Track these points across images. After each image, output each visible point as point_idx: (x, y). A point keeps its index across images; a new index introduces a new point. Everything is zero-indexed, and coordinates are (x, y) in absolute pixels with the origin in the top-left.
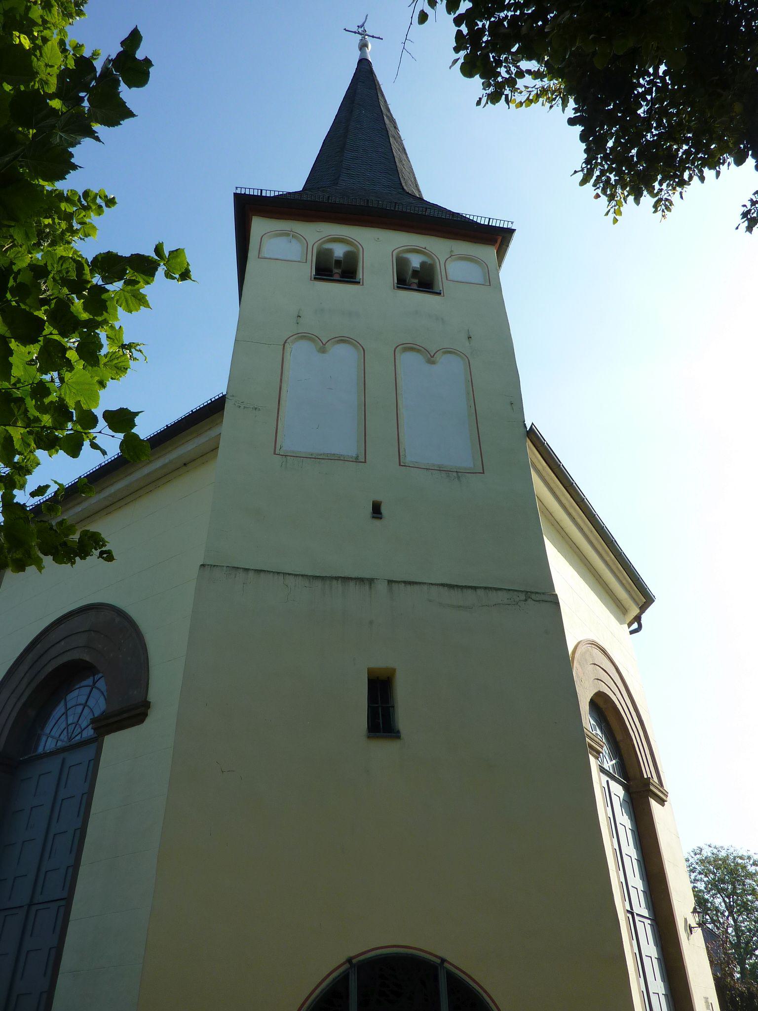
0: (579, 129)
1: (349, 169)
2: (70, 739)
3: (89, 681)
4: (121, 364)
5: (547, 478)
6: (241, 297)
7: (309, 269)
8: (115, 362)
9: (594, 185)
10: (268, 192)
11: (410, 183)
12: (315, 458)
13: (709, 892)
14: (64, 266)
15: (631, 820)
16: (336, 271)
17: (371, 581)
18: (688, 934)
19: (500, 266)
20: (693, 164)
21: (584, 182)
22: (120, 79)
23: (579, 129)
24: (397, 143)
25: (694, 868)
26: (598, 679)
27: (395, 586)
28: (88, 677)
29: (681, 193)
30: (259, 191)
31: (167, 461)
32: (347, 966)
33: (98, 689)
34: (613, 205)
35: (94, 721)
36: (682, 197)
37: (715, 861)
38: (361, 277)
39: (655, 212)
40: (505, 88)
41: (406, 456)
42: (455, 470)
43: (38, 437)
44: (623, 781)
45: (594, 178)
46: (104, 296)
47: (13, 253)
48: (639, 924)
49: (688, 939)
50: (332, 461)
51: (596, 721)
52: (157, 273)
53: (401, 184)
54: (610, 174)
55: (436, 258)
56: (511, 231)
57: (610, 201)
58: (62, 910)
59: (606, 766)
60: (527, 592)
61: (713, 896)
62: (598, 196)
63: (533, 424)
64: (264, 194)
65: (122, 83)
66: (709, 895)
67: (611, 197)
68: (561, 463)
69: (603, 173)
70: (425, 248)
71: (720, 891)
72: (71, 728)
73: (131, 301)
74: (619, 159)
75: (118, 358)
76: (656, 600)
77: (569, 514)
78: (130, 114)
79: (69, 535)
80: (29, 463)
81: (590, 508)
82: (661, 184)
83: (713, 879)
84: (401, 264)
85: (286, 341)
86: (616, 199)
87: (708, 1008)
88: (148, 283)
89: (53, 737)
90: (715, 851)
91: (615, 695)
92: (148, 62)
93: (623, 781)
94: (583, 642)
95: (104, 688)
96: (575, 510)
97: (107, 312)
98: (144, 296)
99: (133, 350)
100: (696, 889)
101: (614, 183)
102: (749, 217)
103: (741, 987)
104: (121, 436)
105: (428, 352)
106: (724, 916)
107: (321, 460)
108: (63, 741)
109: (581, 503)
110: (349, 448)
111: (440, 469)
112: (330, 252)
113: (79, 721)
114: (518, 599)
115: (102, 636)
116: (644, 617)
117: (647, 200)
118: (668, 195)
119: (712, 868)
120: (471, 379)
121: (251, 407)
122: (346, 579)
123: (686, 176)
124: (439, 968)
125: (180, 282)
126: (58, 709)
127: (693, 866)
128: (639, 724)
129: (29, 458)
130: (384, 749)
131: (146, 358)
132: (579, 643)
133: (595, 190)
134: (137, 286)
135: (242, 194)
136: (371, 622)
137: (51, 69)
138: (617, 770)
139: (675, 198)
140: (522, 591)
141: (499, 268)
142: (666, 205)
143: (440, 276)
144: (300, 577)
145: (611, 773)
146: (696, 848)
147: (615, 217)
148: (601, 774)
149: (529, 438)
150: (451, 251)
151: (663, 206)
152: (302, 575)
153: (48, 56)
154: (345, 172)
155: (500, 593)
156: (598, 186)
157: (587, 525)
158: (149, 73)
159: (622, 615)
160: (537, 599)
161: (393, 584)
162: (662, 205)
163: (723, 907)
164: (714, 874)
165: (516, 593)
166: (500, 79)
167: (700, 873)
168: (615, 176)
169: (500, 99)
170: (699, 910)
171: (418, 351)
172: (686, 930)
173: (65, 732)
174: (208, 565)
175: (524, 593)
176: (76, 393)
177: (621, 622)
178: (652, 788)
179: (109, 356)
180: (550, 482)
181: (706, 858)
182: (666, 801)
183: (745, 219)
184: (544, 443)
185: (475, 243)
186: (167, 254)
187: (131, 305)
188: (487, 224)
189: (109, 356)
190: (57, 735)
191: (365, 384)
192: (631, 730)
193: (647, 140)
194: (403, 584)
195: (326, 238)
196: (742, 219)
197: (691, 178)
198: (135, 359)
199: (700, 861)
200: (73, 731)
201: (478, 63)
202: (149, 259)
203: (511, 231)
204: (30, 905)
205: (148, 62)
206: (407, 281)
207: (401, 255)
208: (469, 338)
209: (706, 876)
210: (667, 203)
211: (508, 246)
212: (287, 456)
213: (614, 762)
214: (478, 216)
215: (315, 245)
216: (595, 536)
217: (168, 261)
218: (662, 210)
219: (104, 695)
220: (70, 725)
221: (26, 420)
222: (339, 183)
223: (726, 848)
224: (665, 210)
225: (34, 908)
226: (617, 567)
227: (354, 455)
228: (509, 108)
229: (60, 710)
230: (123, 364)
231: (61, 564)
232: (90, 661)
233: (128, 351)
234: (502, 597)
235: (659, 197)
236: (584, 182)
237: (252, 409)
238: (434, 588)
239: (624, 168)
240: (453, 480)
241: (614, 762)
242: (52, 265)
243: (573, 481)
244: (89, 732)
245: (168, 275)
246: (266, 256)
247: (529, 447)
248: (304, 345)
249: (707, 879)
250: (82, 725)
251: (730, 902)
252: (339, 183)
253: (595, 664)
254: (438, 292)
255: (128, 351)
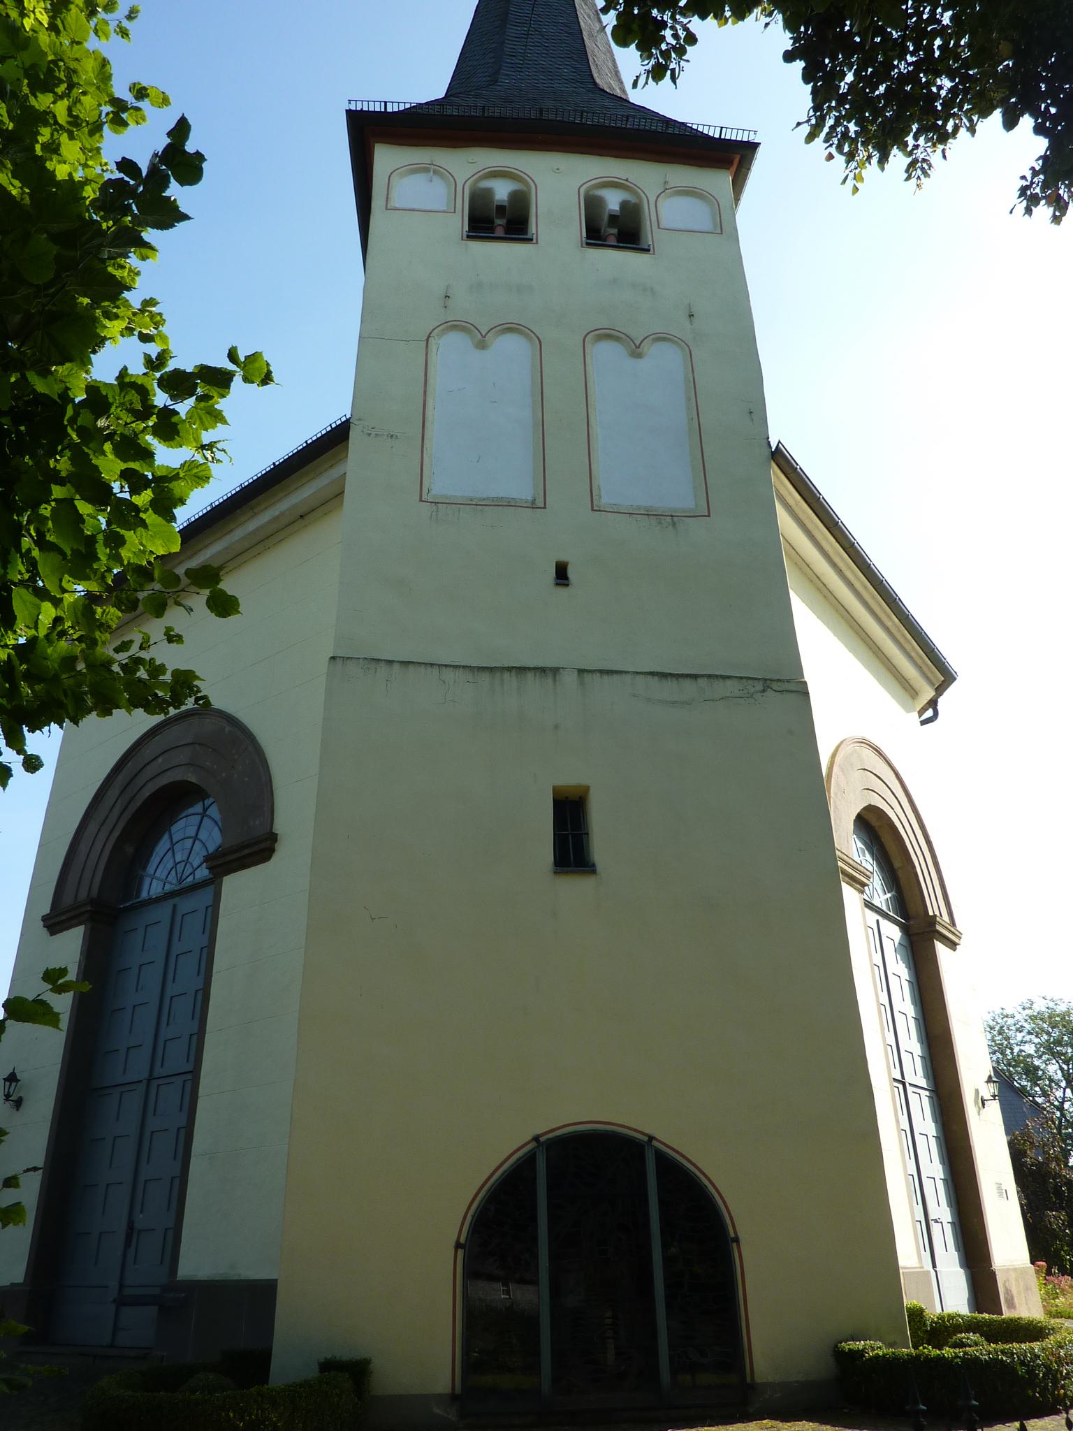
0: (799, 65)
1: (514, 56)
2: (180, 882)
3: (198, 808)
4: (201, 473)
5: (801, 516)
6: (366, 252)
7: (458, 222)
8: (195, 471)
9: (826, 141)
10: (396, 105)
11: (607, 71)
12: (477, 505)
13: (1040, 1057)
14: (127, 398)
15: (909, 967)
16: (498, 222)
17: (555, 671)
18: (979, 1107)
19: (737, 199)
20: (961, 108)
21: (811, 137)
22: (170, 173)
23: (799, 65)
24: (586, 4)
25: (1022, 1026)
26: (868, 789)
27: (587, 677)
28: (197, 802)
29: (943, 151)
30: (383, 104)
31: (277, 513)
32: (534, 1144)
33: (210, 817)
34: (853, 167)
35: (207, 859)
36: (944, 157)
37: (1050, 1017)
38: (534, 231)
39: (908, 178)
40: (670, 60)
41: (600, 497)
42: (669, 514)
43: (118, 599)
44: (900, 919)
45: (826, 130)
46: (175, 419)
47: (66, 369)
48: (911, 1096)
49: (979, 1114)
50: (500, 508)
51: (865, 843)
52: (232, 384)
53: (592, 76)
54: (849, 122)
55: (640, 191)
56: (752, 147)
57: (848, 162)
58: (189, 1085)
59: (876, 902)
60: (766, 680)
61: (1046, 1062)
62: (830, 157)
63: (779, 442)
64: (389, 110)
65: (172, 179)
66: (1041, 1061)
67: (851, 157)
68: (820, 494)
69: (838, 120)
70: (627, 180)
71: (1057, 1055)
72: (180, 868)
73: (206, 419)
74: (859, 103)
75: (197, 467)
76: (958, 678)
77: (834, 565)
78: (185, 217)
79: (159, 676)
80: (108, 617)
81: (863, 556)
82: (916, 138)
83: (1047, 1041)
84: (592, 206)
85: (430, 333)
86: (857, 158)
87: (1001, 1196)
88: (223, 396)
89: (158, 879)
90: (1051, 1005)
91: (893, 809)
92: (199, 157)
93: (900, 919)
94: (847, 741)
95: (217, 816)
96: (842, 558)
97: (179, 436)
98: (220, 412)
99: (214, 450)
100: (1023, 1054)
101: (853, 136)
102: (1029, 193)
103: (1068, 1174)
104: (207, 592)
105: (631, 339)
106: (1060, 1087)
107: (484, 507)
108: (171, 884)
109: (850, 550)
110: (522, 489)
111: (649, 514)
112: (489, 193)
113: (190, 859)
114: (752, 690)
115: (210, 750)
116: (942, 702)
117: (898, 160)
118: (925, 154)
119: (1045, 1026)
120: (694, 378)
121: (385, 434)
122: (521, 670)
123: (950, 127)
124: (646, 1147)
125: (260, 388)
126: (162, 842)
127: (1020, 1024)
128: (926, 846)
129: (109, 612)
130: (575, 887)
131: (231, 458)
132: (842, 742)
133: (826, 149)
134: (211, 402)
135: (358, 111)
136: (556, 727)
137: (79, 46)
138: (892, 905)
139: (936, 158)
140: (760, 679)
141: (736, 207)
142: (923, 169)
143: (648, 223)
144: (461, 669)
145: (882, 910)
146: (1025, 1001)
147: (855, 186)
148: (866, 910)
149: (774, 461)
150: (665, 183)
151: (919, 170)
152: (464, 667)
153: (73, 28)
154: (508, 61)
155: (729, 682)
156: (831, 142)
157: (859, 579)
158: (201, 169)
159: (910, 700)
160: (780, 689)
161: (586, 674)
162: (917, 168)
163: (1059, 1075)
164: (1049, 1034)
165: (750, 682)
166: (664, 47)
167: (1029, 1033)
168: (856, 124)
169: (665, 76)
170: (995, 1079)
171: (617, 339)
172: (976, 1102)
173: (173, 872)
174: (340, 657)
175: (761, 682)
176: (153, 535)
177: (908, 710)
178: (939, 928)
179: (187, 464)
180: (807, 522)
181: (1038, 1013)
182: (959, 944)
183: (1023, 198)
184: (797, 468)
185: (701, 167)
186: (242, 359)
187: (206, 423)
188: (718, 137)
189: (187, 464)
190: (164, 876)
191: (542, 393)
192: (914, 854)
193: (900, 73)
194: (598, 674)
195: (482, 173)
196: (1019, 197)
197: (956, 128)
198: (218, 461)
199: (1030, 1017)
200: (183, 871)
201: (635, 27)
202: (222, 371)
203: (752, 147)
204: (149, 1080)
205: (199, 157)
206: (602, 231)
207: (591, 193)
208: (691, 316)
209: (1037, 1036)
210: (925, 165)
211: (749, 169)
212: (438, 503)
213: (889, 895)
214: (704, 125)
215: (466, 184)
216: (870, 593)
217: (245, 366)
218: (916, 176)
219: (218, 825)
220: (178, 863)
221: (103, 584)
222: (500, 80)
223: (1066, 1000)
224: (922, 177)
225: (155, 1083)
226: (904, 636)
227: (530, 498)
228: (676, 88)
229: (163, 845)
230: (204, 473)
231: (153, 715)
232: (198, 783)
233: (209, 452)
234: (731, 687)
235: (914, 156)
236: (811, 137)
237: (385, 437)
238: (640, 679)
239: (867, 114)
240: (667, 527)
241: (889, 895)
242: (114, 397)
243: (839, 519)
244: (203, 873)
245: (246, 379)
246: (397, 205)
247: (773, 471)
248: (455, 338)
249: (1039, 1040)
250: (193, 864)
251: (1069, 1069)
252: (500, 80)
253: (865, 769)
254: (646, 247)
255: (209, 452)
